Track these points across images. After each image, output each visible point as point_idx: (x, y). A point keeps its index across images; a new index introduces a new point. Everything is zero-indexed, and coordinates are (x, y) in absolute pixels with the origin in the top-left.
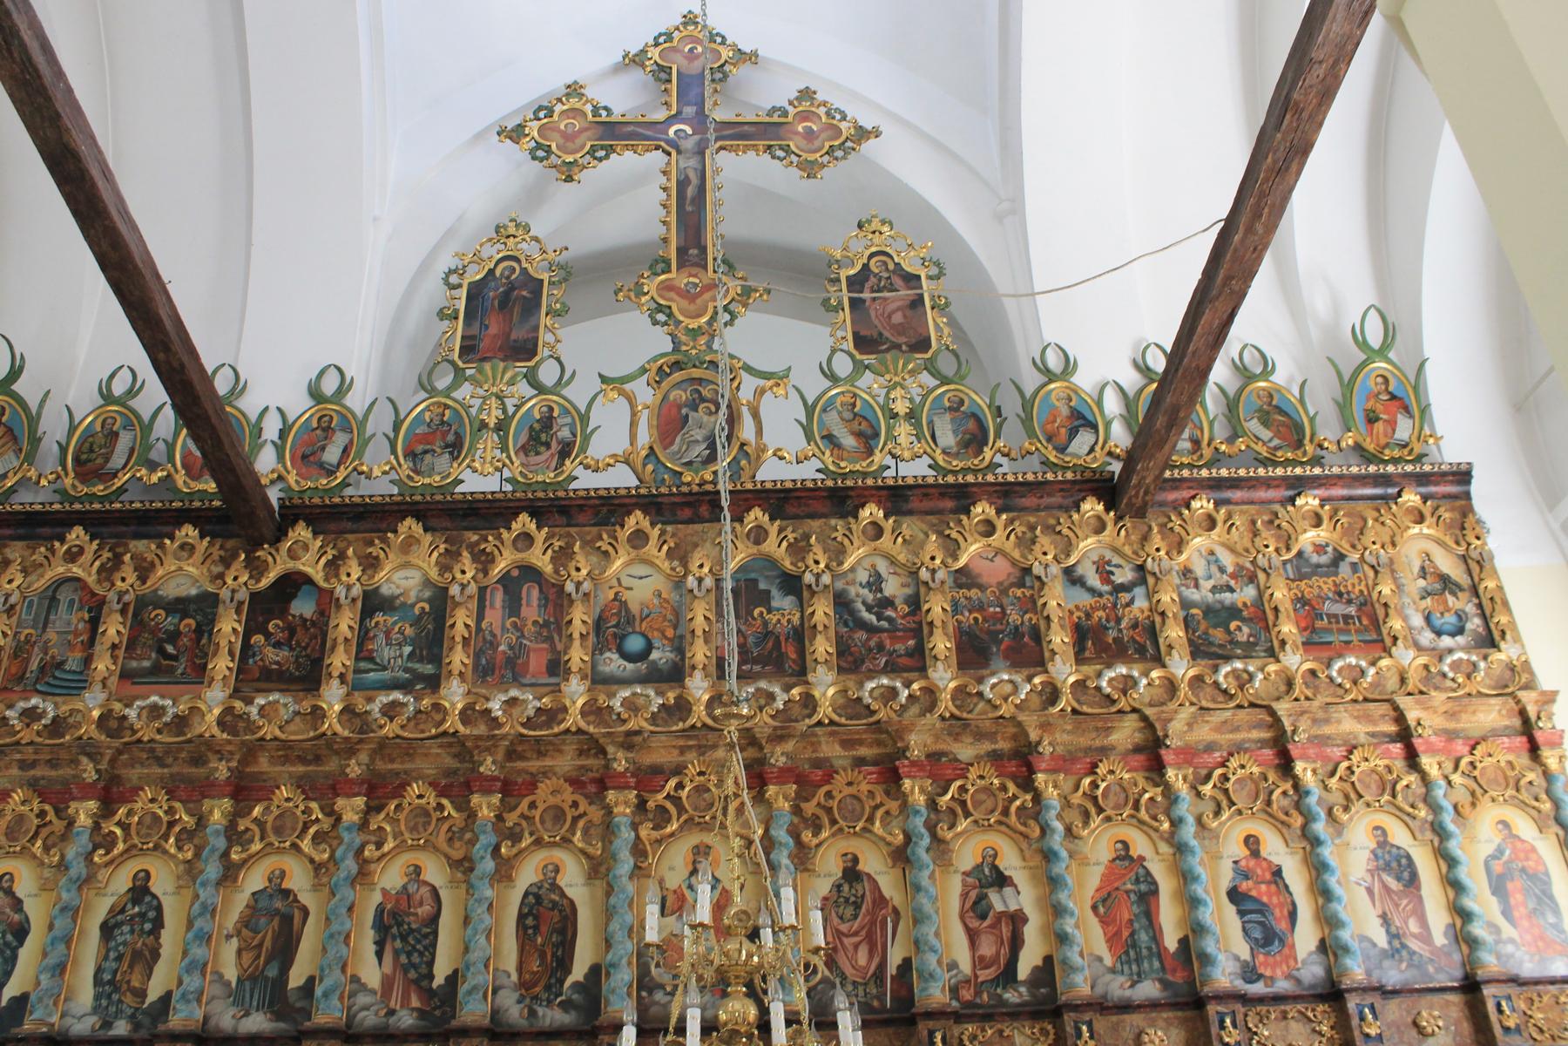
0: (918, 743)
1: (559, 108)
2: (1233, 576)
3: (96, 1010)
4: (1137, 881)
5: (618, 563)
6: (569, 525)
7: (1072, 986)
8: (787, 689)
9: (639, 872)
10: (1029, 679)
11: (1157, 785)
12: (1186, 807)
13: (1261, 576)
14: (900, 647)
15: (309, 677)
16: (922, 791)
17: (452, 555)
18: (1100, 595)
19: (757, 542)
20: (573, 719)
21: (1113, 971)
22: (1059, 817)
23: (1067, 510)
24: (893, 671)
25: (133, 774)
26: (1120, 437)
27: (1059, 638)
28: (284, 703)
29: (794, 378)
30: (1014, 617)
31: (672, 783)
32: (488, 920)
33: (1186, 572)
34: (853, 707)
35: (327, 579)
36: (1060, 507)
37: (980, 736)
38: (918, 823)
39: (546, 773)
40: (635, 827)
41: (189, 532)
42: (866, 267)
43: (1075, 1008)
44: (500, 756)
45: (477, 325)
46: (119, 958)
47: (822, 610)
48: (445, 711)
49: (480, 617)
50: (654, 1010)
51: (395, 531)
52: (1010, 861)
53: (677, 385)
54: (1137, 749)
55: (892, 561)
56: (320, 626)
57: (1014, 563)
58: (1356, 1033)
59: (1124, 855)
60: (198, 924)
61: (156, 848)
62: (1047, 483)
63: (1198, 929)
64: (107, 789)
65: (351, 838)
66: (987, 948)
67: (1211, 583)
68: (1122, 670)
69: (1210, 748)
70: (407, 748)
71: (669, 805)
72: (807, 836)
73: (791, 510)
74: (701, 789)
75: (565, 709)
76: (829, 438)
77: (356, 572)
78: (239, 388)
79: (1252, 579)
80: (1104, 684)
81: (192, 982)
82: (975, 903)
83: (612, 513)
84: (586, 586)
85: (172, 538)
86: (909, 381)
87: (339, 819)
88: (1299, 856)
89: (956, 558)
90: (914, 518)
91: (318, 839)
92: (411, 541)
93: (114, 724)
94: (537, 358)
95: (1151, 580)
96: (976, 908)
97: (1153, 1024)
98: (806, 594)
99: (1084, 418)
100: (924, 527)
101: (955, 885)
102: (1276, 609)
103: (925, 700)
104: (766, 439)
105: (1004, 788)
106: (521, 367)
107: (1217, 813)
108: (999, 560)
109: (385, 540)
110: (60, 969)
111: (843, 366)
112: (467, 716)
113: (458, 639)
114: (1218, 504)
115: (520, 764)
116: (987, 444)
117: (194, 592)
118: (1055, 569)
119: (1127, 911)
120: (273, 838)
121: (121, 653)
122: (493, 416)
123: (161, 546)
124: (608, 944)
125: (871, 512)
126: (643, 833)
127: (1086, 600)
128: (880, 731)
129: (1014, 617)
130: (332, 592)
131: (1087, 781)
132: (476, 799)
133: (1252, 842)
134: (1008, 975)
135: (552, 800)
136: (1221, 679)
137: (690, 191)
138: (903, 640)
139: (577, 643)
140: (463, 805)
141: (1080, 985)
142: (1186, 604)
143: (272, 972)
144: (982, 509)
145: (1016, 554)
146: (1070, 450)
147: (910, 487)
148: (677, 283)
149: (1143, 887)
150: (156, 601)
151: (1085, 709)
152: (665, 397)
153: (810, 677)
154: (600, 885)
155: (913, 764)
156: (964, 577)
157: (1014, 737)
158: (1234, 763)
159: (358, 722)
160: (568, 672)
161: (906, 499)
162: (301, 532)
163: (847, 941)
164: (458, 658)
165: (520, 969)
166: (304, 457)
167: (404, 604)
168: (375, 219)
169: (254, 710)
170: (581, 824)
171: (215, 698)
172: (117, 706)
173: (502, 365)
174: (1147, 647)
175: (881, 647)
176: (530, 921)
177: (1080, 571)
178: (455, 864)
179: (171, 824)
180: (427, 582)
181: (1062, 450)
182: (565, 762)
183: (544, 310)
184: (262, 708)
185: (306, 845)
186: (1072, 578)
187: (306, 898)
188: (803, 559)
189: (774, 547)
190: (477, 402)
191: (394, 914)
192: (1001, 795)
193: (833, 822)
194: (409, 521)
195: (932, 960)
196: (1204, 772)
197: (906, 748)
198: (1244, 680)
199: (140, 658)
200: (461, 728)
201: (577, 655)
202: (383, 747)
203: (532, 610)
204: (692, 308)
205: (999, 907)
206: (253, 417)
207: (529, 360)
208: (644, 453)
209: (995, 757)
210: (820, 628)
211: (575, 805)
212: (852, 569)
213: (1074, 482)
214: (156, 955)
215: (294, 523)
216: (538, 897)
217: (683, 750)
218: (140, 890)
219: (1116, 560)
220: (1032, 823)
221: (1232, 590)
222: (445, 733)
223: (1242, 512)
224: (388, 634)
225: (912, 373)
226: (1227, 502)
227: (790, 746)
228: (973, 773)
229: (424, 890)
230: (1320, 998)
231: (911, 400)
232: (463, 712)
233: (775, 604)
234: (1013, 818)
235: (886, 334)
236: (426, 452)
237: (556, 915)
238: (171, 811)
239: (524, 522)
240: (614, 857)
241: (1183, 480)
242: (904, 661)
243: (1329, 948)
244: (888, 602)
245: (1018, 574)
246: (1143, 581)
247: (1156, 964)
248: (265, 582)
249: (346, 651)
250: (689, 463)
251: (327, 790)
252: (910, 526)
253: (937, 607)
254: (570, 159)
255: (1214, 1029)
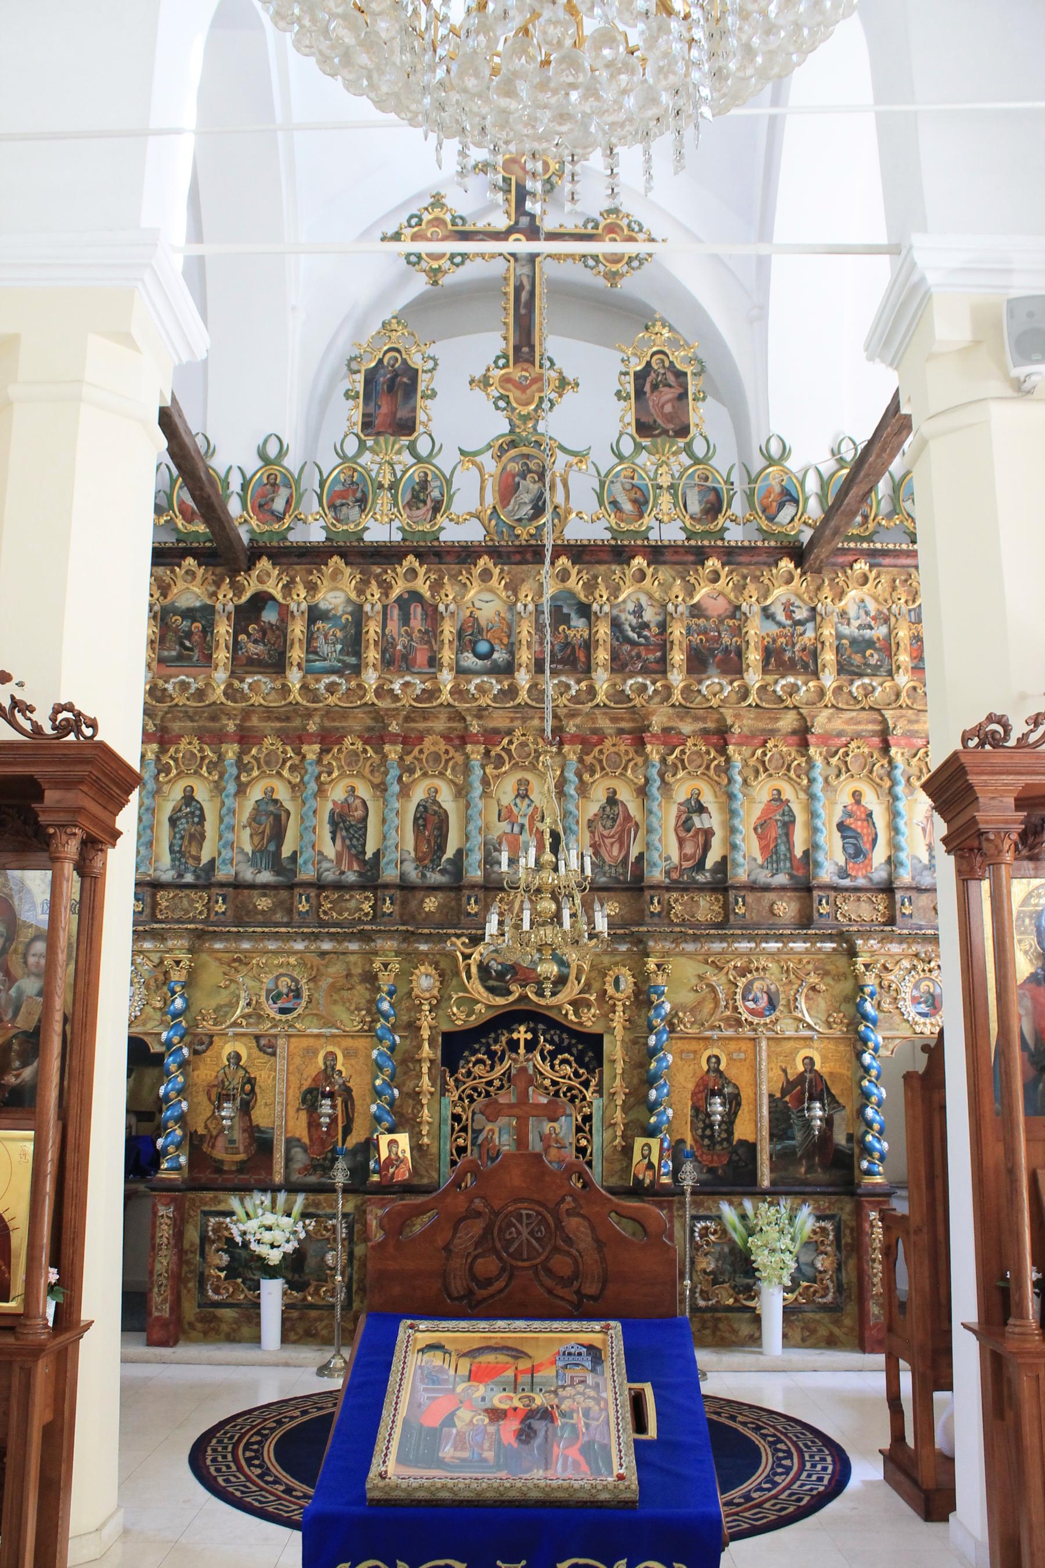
0: (657, 722)
1: (427, 217)
2: (874, 618)
3: (173, 867)
4: (783, 815)
5: (472, 593)
6: (440, 563)
7: (736, 875)
8: (578, 682)
9: (485, 794)
10: (731, 683)
11: (803, 756)
12: (818, 773)
13: (893, 620)
14: (651, 657)
15: (278, 665)
16: (658, 752)
17: (365, 583)
18: (784, 627)
19: (563, 581)
20: (445, 697)
21: (762, 866)
22: (740, 773)
23: (769, 565)
24: (646, 673)
25: (176, 726)
26: (814, 510)
27: (754, 656)
28: (265, 682)
29: (593, 456)
30: (726, 639)
31: (506, 741)
32: (397, 821)
33: (843, 614)
34: (619, 696)
35: (284, 598)
36: (765, 564)
37: (696, 719)
38: (654, 773)
39: (429, 731)
40: (483, 767)
41: (190, 562)
42: (648, 364)
43: (737, 888)
44: (400, 721)
45: (372, 404)
46: (182, 838)
47: (603, 630)
48: (365, 690)
49: (384, 626)
50: (493, 876)
51: (326, 564)
52: (708, 799)
53: (512, 459)
54: (794, 732)
55: (651, 597)
56: (281, 630)
57: (730, 602)
58: (898, 913)
59: (778, 798)
60: (226, 820)
61: (196, 772)
62: (756, 548)
63: (815, 846)
64: (162, 737)
65: (312, 770)
66: (689, 850)
67: (859, 622)
68: (791, 679)
69: (840, 734)
70: (344, 714)
71: (503, 754)
72: (586, 777)
73: (587, 558)
74: (524, 745)
75: (440, 691)
76: (614, 503)
77: (303, 594)
78: (211, 451)
79: (886, 620)
80: (778, 689)
81: (227, 854)
82: (685, 822)
83: (468, 556)
84: (452, 607)
85: (180, 566)
86: (672, 459)
87: (304, 757)
88: (884, 806)
89: (692, 597)
90: (667, 567)
91: (293, 769)
92: (337, 572)
93: (159, 694)
94: (416, 434)
95: (818, 619)
96: (685, 825)
97: (781, 899)
98: (593, 618)
99: (790, 495)
100: (673, 573)
101: (674, 811)
102: (898, 644)
103: (664, 694)
104: (571, 504)
105: (708, 753)
106: (405, 441)
107: (838, 776)
108: (721, 599)
109: (320, 571)
110: (149, 844)
111: (627, 447)
112: (379, 692)
113: (371, 642)
114: (871, 566)
115: (413, 725)
116: (720, 511)
117: (198, 604)
118: (756, 608)
119: (776, 831)
120: (265, 768)
121: (157, 646)
122: (386, 480)
123: (173, 571)
124: (467, 838)
125: (639, 562)
126: (488, 771)
127: (774, 630)
128: (634, 713)
129: (726, 639)
130: (288, 606)
131: (759, 752)
132: (387, 748)
133: (857, 796)
134: (700, 866)
135: (433, 749)
136: (854, 690)
137: (524, 296)
138: (654, 651)
139: (446, 646)
140: (379, 750)
141: (741, 875)
142: (839, 636)
143: (272, 848)
144: (713, 563)
145: (732, 596)
146: (777, 520)
147: (665, 547)
148: (513, 376)
149: (786, 818)
150: (176, 611)
151: (764, 705)
152: (504, 468)
153: (593, 675)
154: (462, 802)
155: (653, 736)
156: (697, 611)
157: (718, 721)
158: (853, 745)
159: (310, 694)
160: (441, 665)
161: (662, 554)
162: (264, 563)
163: (608, 841)
164: (372, 655)
165: (416, 850)
166: (261, 506)
167: (335, 616)
168: (294, 308)
169: (246, 686)
170: (451, 764)
171: (221, 676)
172: (160, 682)
173: (392, 438)
174: (810, 665)
175: (639, 656)
176: (421, 822)
177: (773, 609)
178: (375, 786)
179: (203, 758)
180: (349, 601)
181: (771, 519)
182: (440, 724)
183: (419, 394)
184: (250, 684)
185: (285, 773)
186: (767, 614)
187: (288, 805)
188: (592, 594)
189: (575, 585)
190: (375, 467)
191: (340, 815)
192: (706, 757)
193: (603, 769)
194: (336, 558)
195: (655, 855)
196: (834, 749)
197: (650, 725)
198: (868, 692)
199: (169, 649)
200: (376, 701)
201: (447, 655)
202: (329, 712)
203: (417, 623)
204: (524, 397)
205: (698, 825)
206: (222, 474)
207: (410, 435)
208: (489, 512)
209: (705, 733)
210: (601, 642)
211: (447, 752)
212: (624, 601)
213: (776, 548)
214: (203, 837)
215: (259, 558)
216: (425, 807)
217: (512, 720)
218: (189, 798)
219: (798, 603)
220: (723, 775)
221: (871, 628)
222: (366, 704)
223: (888, 573)
224: (326, 636)
225: (674, 454)
226: (880, 565)
227: (578, 720)
228: (690, 742)
229: (358, 801)
230: (882, 890)
231: (672, 476)
232: (376, 691)
233: (573, 623)
234: (712, 771)
235: (659, 421)
236: (342, 505)
237: (436, 819)
238: (201, 750)
239: (410, 561)
240: (470, 785)
241: (849, 549)
242: (653, 666)
243: (892, 862)
244: (646, 626)
245: (731, 609)
246: (813, 618)
247: (788, 864)
248: (244, 599)
249: (301, 648)
250: (520, 520)
251: (297, 739)
252: (664, 573)
253: (677, 631)
254: (435, 266)
255: (815, 905)
